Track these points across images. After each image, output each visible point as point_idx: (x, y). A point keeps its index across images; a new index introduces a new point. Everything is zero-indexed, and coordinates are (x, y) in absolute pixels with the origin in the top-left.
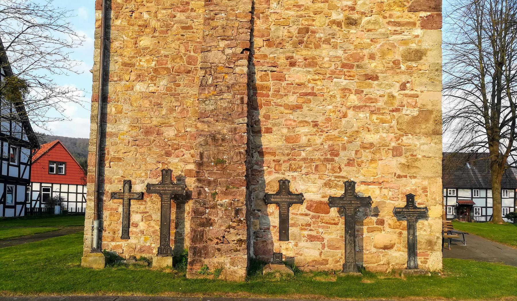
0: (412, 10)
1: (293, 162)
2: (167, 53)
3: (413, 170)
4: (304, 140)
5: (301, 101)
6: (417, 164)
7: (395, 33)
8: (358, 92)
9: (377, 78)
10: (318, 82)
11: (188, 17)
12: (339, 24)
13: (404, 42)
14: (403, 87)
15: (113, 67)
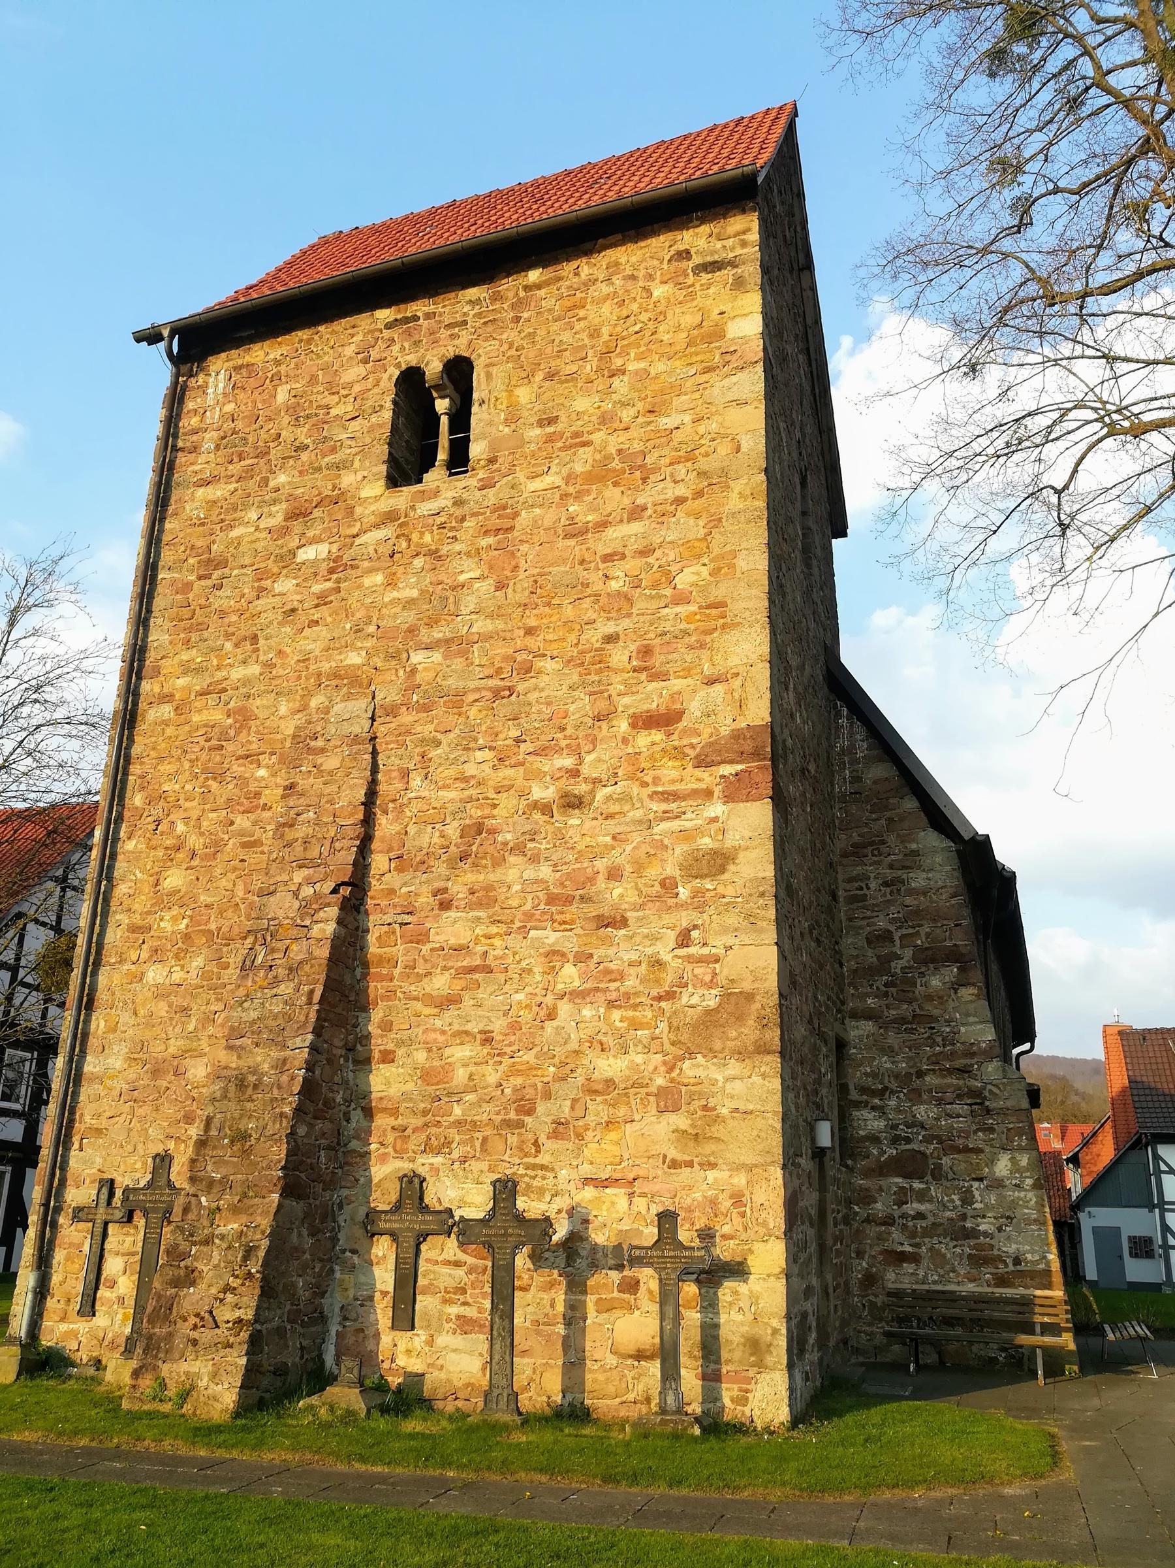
0: (702, 762)
1: (433, 1130)
2: (209, 900)
3: (708, 1148)
4: (460, 1075)
5: (458, 985)
6: (717, 1131)
7: (667, 816)
8: (582, 957)
9: (623, 923)
10: (497, 942)
11: (255, 823)
12: (546, 809)
13: (685, 835)
14: (684, 940)
15: (113, 936)
